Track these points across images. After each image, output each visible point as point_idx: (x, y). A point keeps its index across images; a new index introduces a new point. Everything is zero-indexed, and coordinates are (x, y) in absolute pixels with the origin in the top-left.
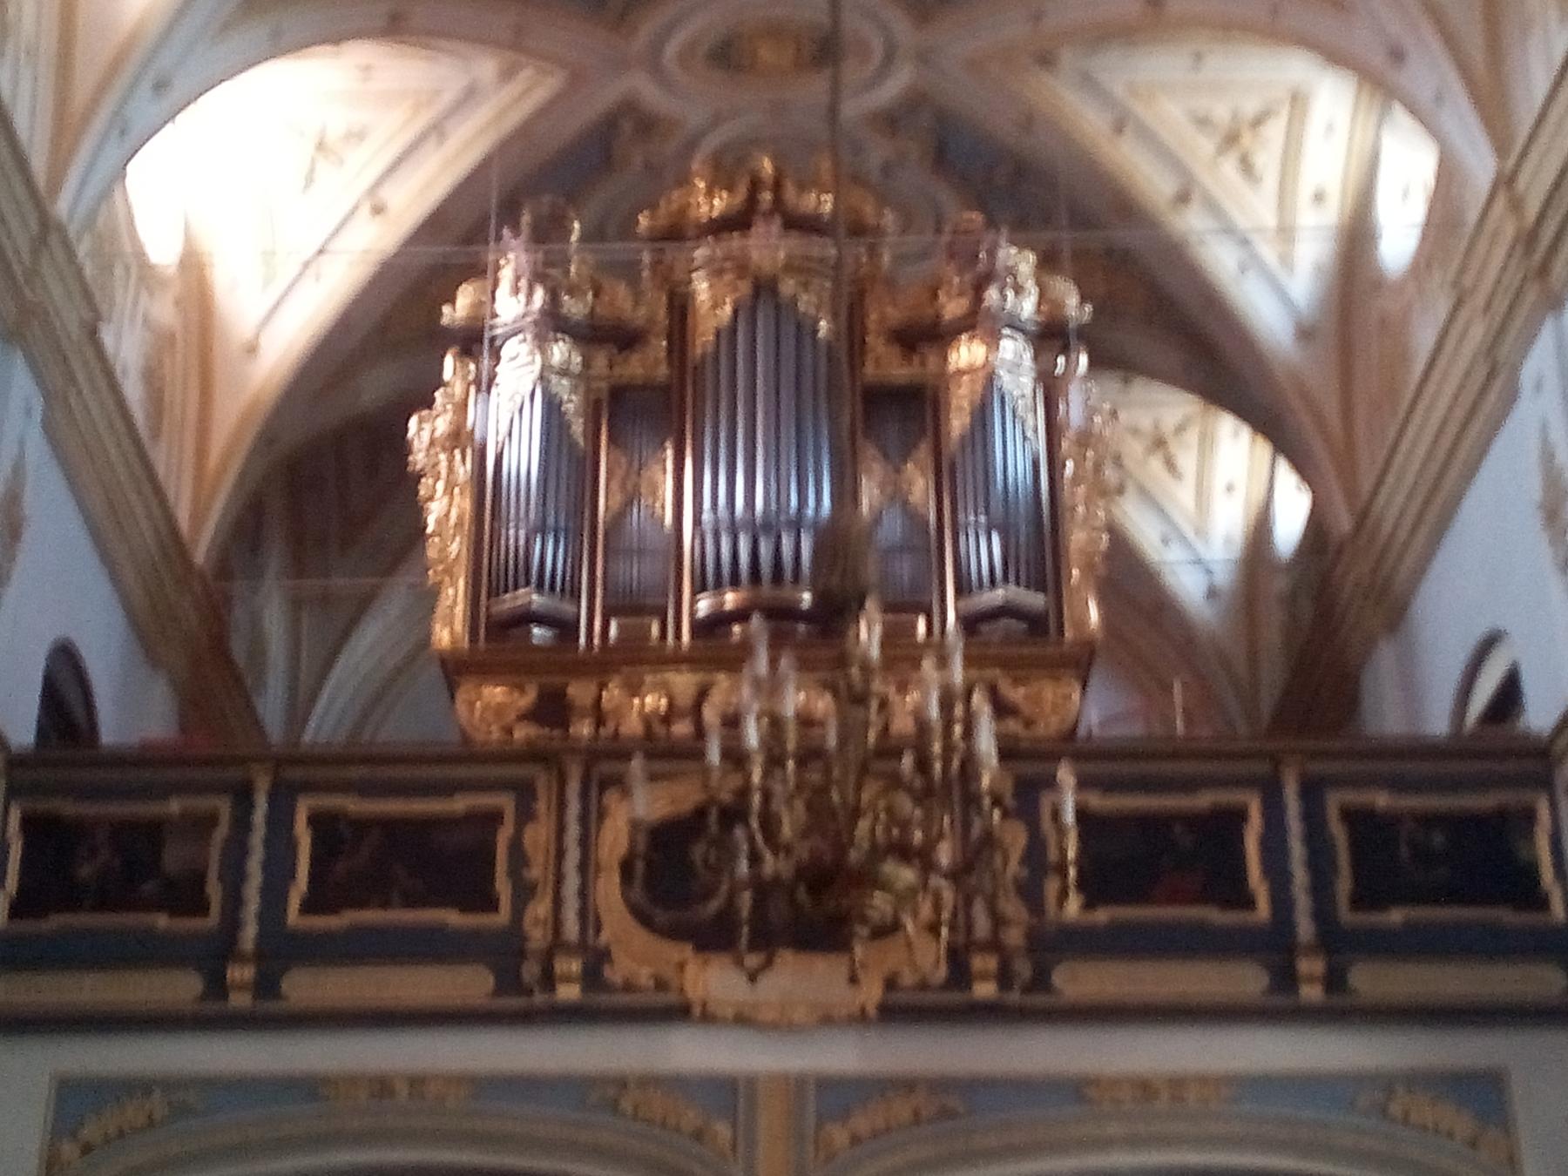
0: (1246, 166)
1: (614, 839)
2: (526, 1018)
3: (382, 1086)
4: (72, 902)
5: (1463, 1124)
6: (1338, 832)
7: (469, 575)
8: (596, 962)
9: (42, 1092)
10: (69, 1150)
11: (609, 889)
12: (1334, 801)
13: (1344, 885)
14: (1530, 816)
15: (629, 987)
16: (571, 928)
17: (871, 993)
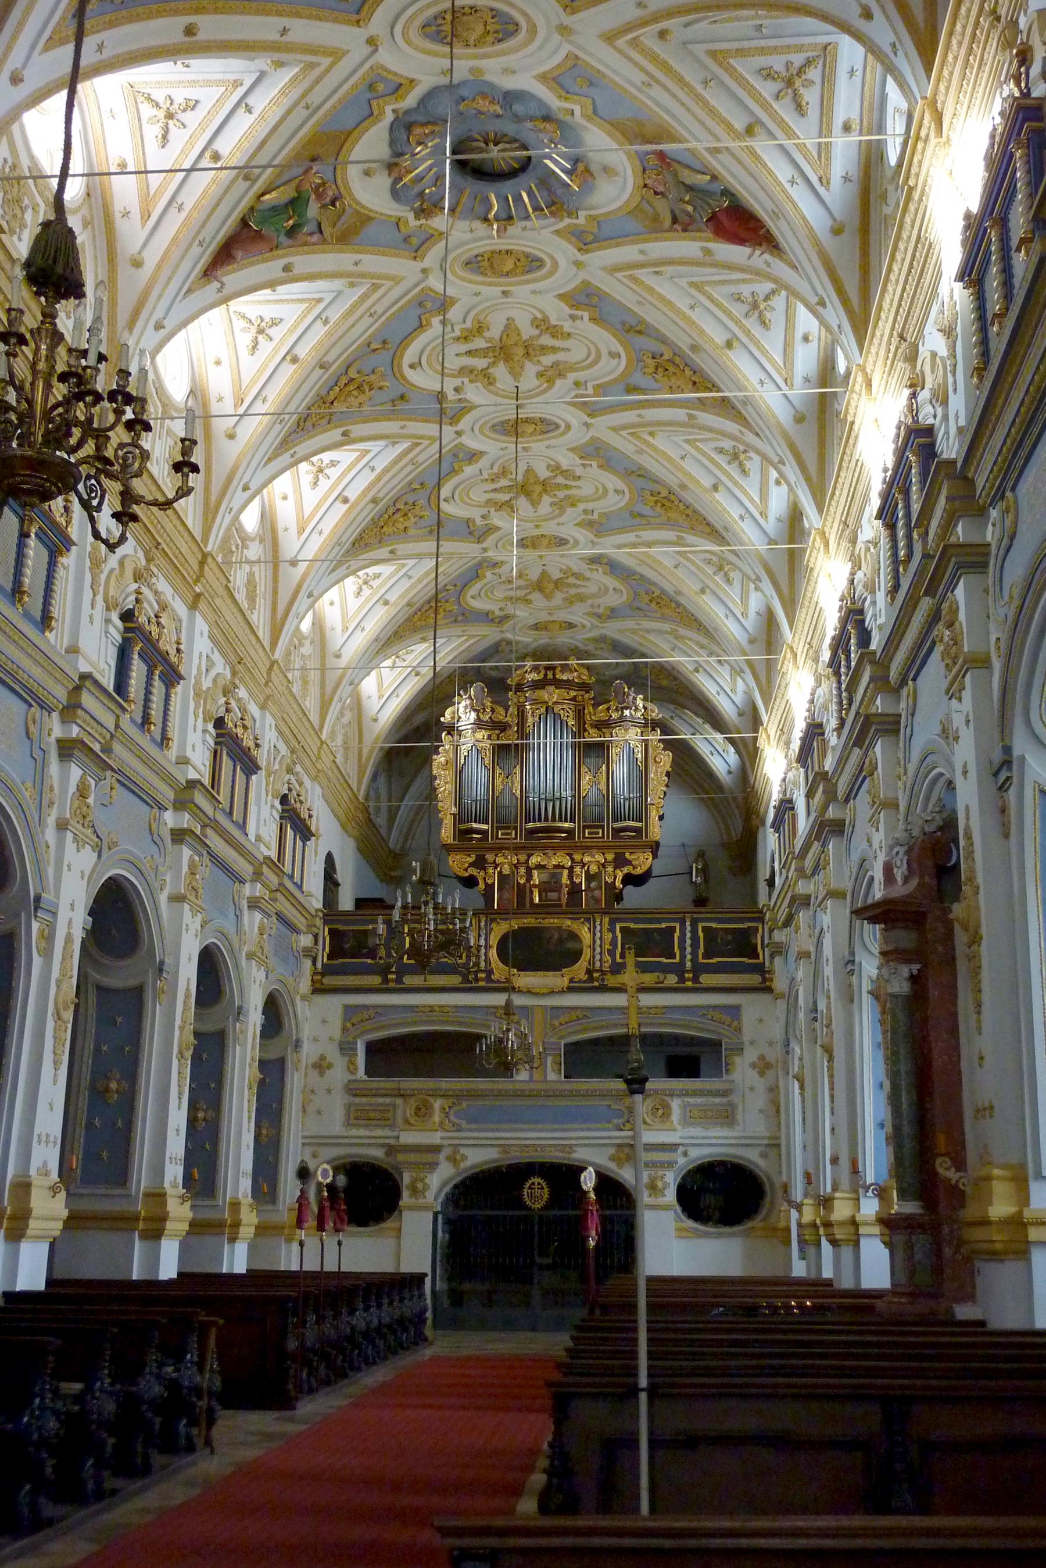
1: (494, 941)
2: (471, 990)
3: (431, 1009)
4: (344, 956)
5: (728, 1020)
6: (701, 934)
7: (246, 144)
8: (490, 972)
9: (340, 1010)
10: (349, 1025)
11: (493, 953)
12: (700, 926)
13: (701, 950)
14: (757, 928)
15: (498, 981)
16: (483, 964)
17: (565, 982)
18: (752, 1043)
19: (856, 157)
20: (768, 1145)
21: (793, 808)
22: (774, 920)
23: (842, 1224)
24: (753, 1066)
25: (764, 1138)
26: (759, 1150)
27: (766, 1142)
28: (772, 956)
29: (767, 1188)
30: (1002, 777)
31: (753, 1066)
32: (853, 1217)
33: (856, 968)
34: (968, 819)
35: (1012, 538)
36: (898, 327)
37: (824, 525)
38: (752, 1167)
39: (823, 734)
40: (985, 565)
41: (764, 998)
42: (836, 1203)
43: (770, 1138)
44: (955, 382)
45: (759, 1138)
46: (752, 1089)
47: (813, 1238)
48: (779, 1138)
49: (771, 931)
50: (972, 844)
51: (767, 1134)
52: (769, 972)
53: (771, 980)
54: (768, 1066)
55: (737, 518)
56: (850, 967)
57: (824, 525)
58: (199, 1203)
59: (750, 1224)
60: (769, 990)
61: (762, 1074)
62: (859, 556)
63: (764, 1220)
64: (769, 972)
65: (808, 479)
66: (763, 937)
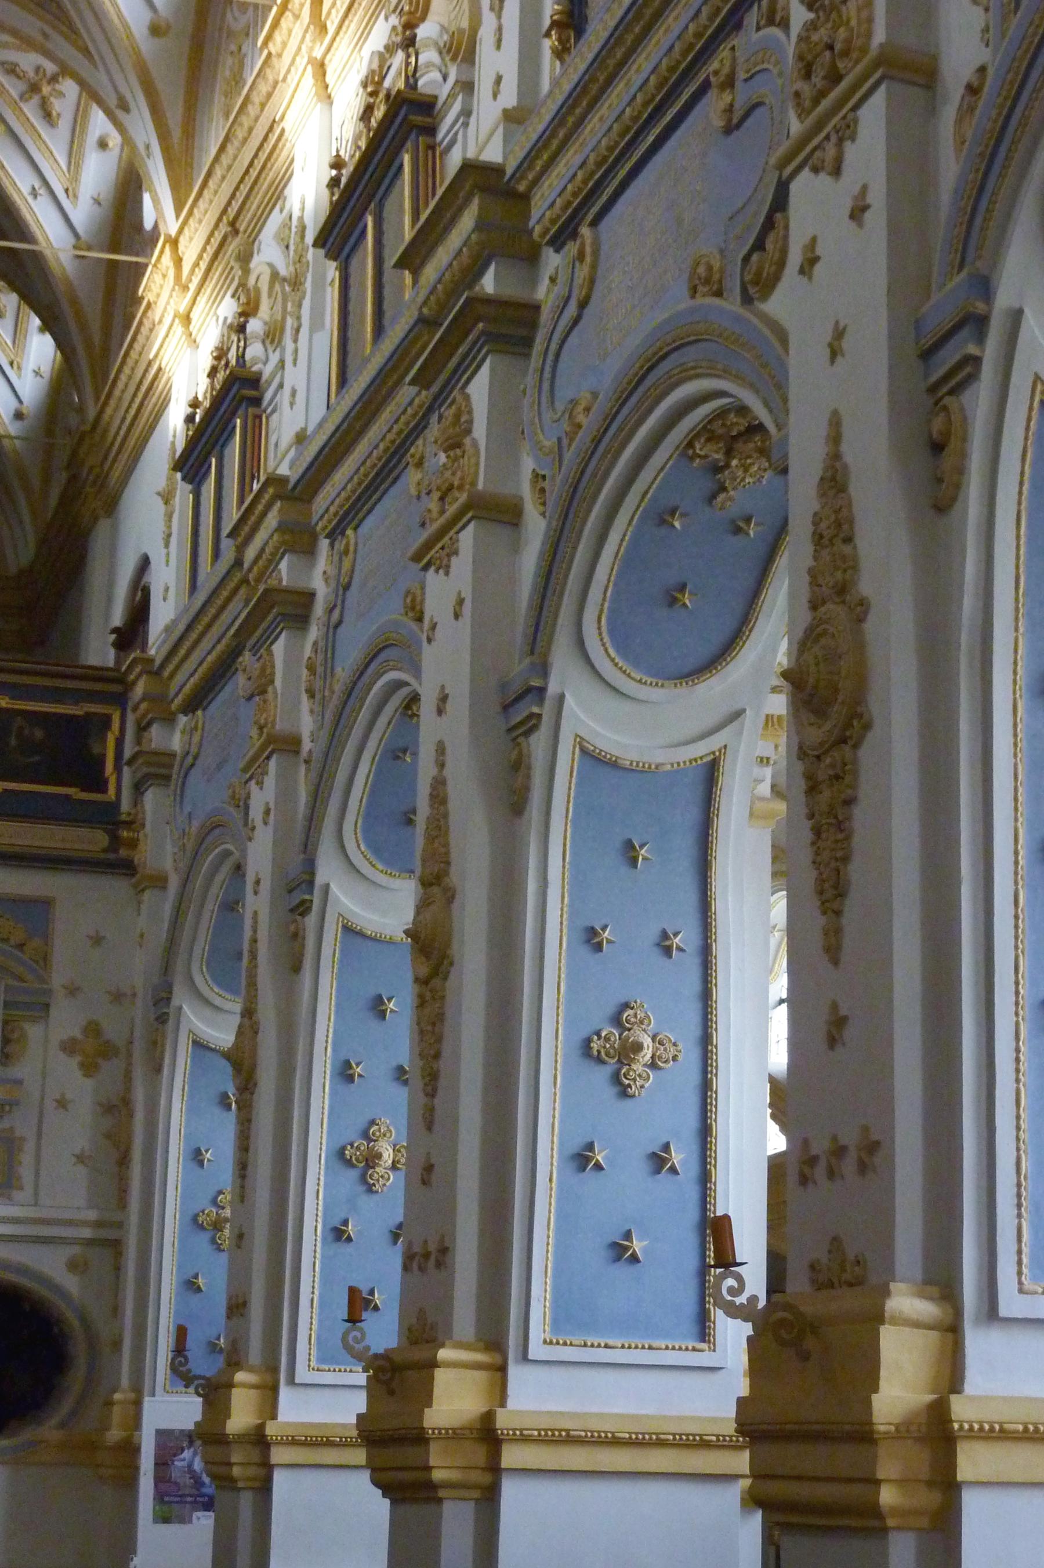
0: (47, 115)
18: (73, 991)
19: (116, 167)
20: (90, 1243)
21: (257, 401)
22: (157, 699)
23: (454, 1435)
24: (69, 1047)
25: (84, 1223)
26: (66, 1253)
27: (87, 1233)
28: (138, 789)
29: (79, 1351)
30: (949, 357)
31: (69, 1047)
32: (488, 1418)
33: (547, 712)
34: (255, 931)
35: (583, 305)
36: (232, 212)
37: (180, 231)
38: (44, 1292)
39: (431, 131)
40: (528, 342)
41: (116, 887)
42: (441, 1376)
43: (98, 1224)
44: (296, 351)
45: (70, 1223)
46: (62, 1104)
47: (252, 1471)
48: (120, 1225)
49: (142, 728)
50: (256, 966)
51: (92, 1215)
52: (129, 824)
53: (133, 844)
54: (107, 1051)
55: (25, 190)
56: (298, 897)
57: (180, 231)
58: (855, 1491)
59: (28, 1434)
60: (127, 868)
61: (89, 1068)
62: (257, 290)
63: (62, 1425)
64: (129, 824)
65: (164, 136)
66: (120, 742)
